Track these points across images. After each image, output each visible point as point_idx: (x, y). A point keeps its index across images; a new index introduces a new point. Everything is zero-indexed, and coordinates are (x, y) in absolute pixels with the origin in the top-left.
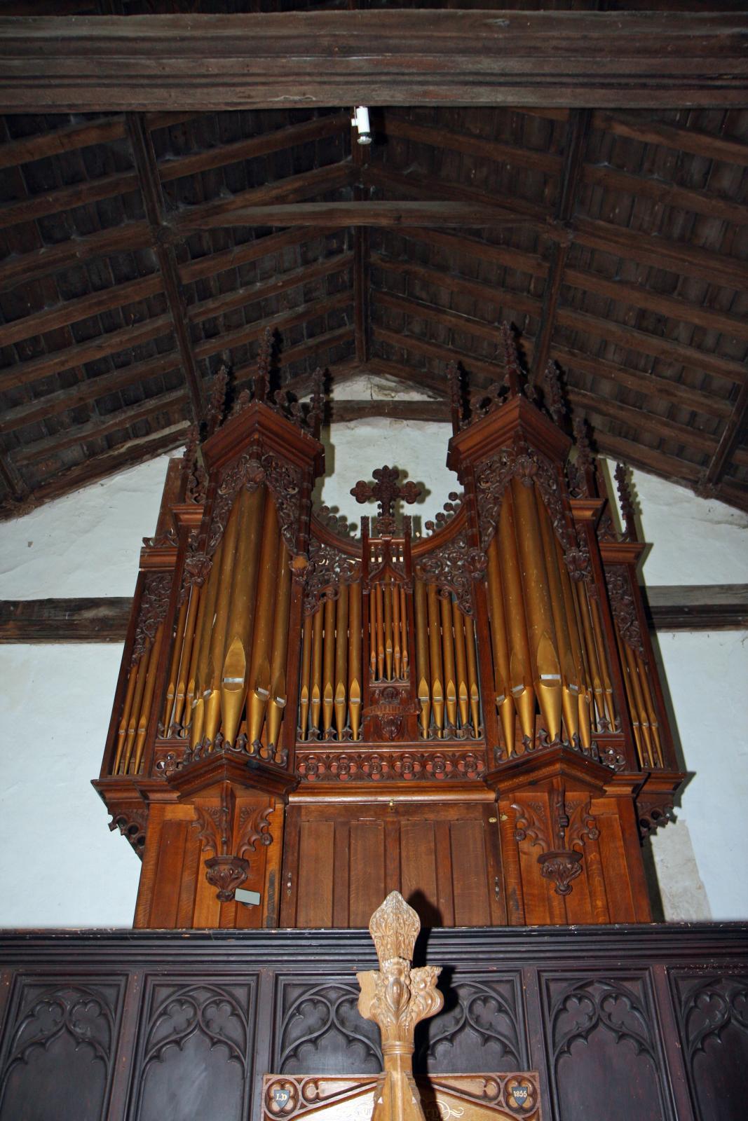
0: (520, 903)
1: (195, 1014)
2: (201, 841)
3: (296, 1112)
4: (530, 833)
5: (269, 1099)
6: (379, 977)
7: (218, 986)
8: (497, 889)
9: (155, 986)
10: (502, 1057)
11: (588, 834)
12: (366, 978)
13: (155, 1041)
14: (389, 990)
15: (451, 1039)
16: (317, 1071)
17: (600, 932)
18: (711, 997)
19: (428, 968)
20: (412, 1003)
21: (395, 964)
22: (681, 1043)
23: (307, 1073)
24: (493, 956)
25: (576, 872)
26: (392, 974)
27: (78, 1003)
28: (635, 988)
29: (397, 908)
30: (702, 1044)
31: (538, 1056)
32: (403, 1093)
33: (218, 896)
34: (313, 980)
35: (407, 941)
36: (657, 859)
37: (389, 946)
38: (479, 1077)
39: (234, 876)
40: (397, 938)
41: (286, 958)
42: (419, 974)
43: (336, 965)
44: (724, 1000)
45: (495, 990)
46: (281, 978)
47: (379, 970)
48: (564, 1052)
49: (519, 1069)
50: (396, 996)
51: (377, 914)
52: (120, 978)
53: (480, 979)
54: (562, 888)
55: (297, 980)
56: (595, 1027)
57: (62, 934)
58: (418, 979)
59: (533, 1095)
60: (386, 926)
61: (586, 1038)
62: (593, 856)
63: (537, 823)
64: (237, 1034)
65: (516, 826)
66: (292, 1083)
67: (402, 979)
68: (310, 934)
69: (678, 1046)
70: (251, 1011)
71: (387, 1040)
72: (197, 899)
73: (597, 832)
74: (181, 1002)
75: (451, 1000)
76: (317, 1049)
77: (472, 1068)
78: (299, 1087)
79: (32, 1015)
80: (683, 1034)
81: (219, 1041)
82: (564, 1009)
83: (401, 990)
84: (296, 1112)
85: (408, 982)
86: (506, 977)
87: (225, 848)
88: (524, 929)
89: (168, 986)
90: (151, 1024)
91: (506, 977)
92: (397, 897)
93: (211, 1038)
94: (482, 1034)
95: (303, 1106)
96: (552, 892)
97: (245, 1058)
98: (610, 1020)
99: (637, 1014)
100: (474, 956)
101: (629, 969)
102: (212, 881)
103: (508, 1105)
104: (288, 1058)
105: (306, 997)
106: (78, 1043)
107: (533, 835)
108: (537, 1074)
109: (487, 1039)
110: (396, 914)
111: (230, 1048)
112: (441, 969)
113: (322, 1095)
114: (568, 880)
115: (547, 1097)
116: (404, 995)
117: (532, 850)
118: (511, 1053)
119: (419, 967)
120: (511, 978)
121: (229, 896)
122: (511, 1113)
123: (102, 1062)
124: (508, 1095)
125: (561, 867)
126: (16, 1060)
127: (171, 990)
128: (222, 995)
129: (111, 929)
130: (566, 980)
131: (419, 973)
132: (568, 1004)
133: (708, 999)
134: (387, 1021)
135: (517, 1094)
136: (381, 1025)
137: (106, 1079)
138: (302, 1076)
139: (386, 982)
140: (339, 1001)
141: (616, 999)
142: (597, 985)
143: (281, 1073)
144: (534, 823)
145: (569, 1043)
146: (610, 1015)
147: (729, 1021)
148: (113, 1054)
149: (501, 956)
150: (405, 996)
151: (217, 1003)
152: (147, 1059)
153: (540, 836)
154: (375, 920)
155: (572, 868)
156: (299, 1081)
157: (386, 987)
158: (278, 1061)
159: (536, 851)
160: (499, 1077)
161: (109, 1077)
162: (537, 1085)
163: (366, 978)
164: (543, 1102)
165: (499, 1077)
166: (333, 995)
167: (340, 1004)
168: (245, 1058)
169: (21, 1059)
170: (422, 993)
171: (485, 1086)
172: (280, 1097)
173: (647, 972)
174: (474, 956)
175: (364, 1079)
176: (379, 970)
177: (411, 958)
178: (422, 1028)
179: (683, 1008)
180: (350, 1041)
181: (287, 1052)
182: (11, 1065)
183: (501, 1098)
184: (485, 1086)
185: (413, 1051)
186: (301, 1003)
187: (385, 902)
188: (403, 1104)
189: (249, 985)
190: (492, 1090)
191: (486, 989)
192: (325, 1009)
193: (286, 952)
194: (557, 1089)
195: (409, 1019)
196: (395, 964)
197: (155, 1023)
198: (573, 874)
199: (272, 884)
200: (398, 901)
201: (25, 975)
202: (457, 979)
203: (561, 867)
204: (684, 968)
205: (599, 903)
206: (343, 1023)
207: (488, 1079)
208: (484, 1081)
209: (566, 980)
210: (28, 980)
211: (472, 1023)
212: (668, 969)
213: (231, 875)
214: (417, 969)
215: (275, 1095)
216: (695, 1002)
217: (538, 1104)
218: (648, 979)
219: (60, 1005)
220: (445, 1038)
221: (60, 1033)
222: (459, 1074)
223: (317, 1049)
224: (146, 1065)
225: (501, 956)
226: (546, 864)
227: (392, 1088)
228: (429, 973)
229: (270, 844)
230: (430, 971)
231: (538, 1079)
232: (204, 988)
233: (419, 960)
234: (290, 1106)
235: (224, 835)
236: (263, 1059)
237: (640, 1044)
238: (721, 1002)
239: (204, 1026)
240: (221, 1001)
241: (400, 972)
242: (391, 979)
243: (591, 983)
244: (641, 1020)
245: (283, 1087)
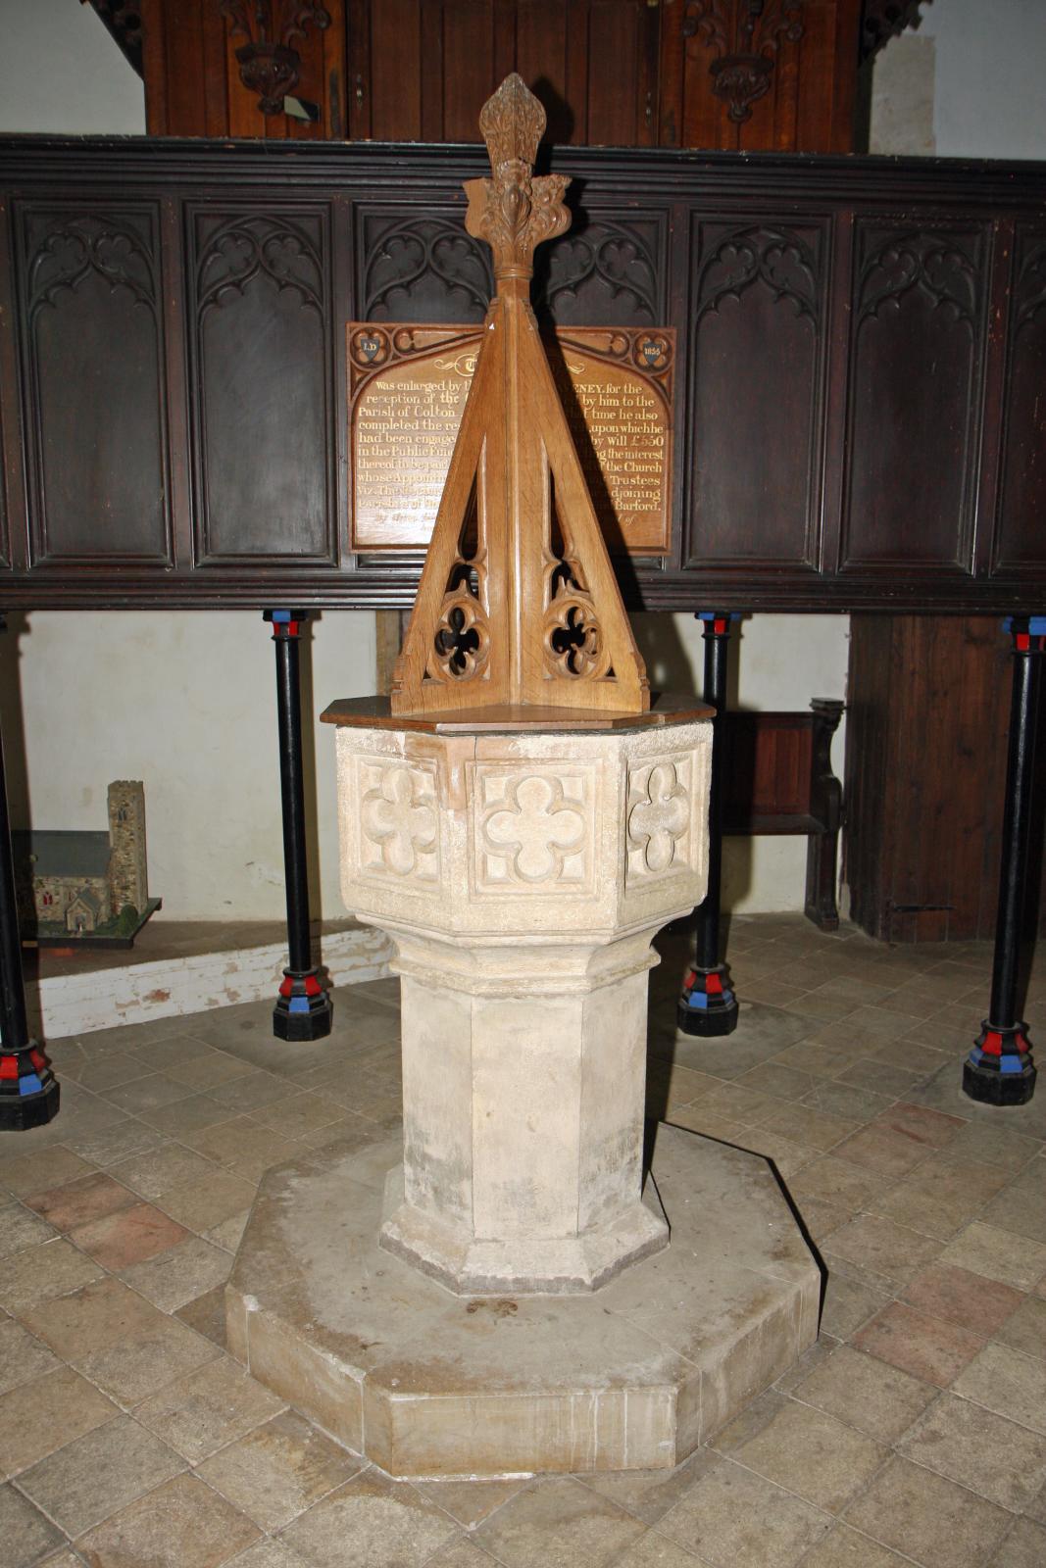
0: (678, 132)
1: (254, 250)
2: (224, 19)
3: (387, 364)
4: (705, 25)
5: (355, 349)
6: (492, 187)
7: (277, 216)
8: (648, 111)
9: (197, 216)
10: (635, 311)
11: (787, 31)
12: (475, 189)
13: (208, 283)
14: (506, 200)
15: (576, 287)
16: (412, 320)
17: (778, 162)
18: (900, 255)
19: (553, 177)
20: (532, 220)
21: (513, 167)
22: (852, 306)
23: (399, 321)
24: (636, 188)
25: (761, 88)
26: (509, 180)
27: (102, 237)
28: (810, 239)
29: (518, 101)
30: (876, 307)
31: (679, 310)
32: (518, 321)
33: (261, 107)
34: (402, 211)
35: (528, 142)
36: (877, 98)
37: (505, 147)
38: (606, 331)
39: (279, 75)
40: (516, 136)
41: (365, 182)
42: (541, 185)
43: (430, 192)
44: (916, 260)
45: (634, 232)
46: (360, 207)
47: (491, 178)
48: (711, 309)
49: (655, 325)
50: (513, 206)
51: (490, 104)
52: (149, 204)
53: (617, 218)
54: (738, 112)
55: (380, 211)
56: (751, 282)
57: (58, 140)
58: (540, 190)
59: (667, 353)
60: (501, 119)
61: (739, 295)
62: (788, 68)
63: (716, 10)
64: (311, 277)
65: (685, 13)
66: (381, 332)
67: (522, 187)
68: (396, 147)
69: (848, 307)
70: (326, 249)
71: (501, 262)
72: (231, 111)
73: (801, 29)
74: (235, 238)
75: (580, 223)
76: (410, 295)
77: (595, 322)
78: (391, 337)
79: (45, 250)
80: (856, 295)
81: (288, 284)
82: (718, 259)
83: (520, 200)
84: (387, 364)
85: (528, 193)
86: (648, 215)
87: (263, 31)
88: (679, 152)
89: (215, 216)
90: (200, 263)
91: (648, 215)
92: (516, 81)
93: (279, 281)
94: (613, 284)
95: (395, 357)
96: (724, 118)
97: (322, 303)
98: (772, 275)
99: (806, 270)
100: (611, 187)
101: (807, 215)
102: (250, 82)
103: (636, 362)
104: (374, 305)
105: (393, 232)
106: (113, 285)
107: (709, 29)
108: (675, 331)
109: (618, 290)
110: (515, 103)
111: (304, 293)
112: (570, 181)
113: (417, 346)
114: (749, 99)
115: (683, 356)
116: (523, 205)
117: (704, 54)
118: (646, 307)
119: (543, 175)
120: (656, 218)
121: (275, 106)
122: (639, 371)
123: (146, 307)
124: (637, 352)
125: (741, 80)
126: (40, 302)
127: (218, 222)
128: (286, 229)
129: (127, 136)
130: (724, 223)
131: (542, 184)
132: (723, 254)
133: (896, 256)
134: (501, 241)
135: (648, 351)
136: (493, 245)
137: (156, 324)
138: (393, 325)
139: (501, 191)
140: (436, 239)
141: (784, 250)
142: (763, 232)
143: (367, 321)
144: (712, 10)
145: (718, 299)
146: (772, 271)
147: (915, 283)
148: (158, 298)
149: (646, 188)
150: (523, 212)
151: (281, 238)
152: (202, 304)
153: (718, 30)
154: (487, 112)
155: (757, 82)
156: (390, 331)
157: (502, 197)
158: (363, 309)
159: (708, 55)
160: (629, 333)
161: (160, 323)
162: (673, 343)
163: (475, 189)
164: (677, 363)
165: (629, 333)
166: (428, 232)
167: (437, 243)
168: (322, 303)
169: (47, 300)
170: (545, 208)
171: (612, 342)
172: (368, 346)
173: (828, 220)
174: (611, 187)
175: (467, 330)
176: (491, 178)
177: (534, 162)
178: (544, 253)
179: (864, 263)
180: (451, 286)
181: (372, 298)
182: (35, 308)
183: (629, 355)
184: (612, 342)
185: (531, 275)
186: (388, 240)
187: (500, 89)
188: (518, 332)
189: (319, 216)
190: (619, 345)
191: (620, 228)
192: (419, 249)
193: (365, 173)
194: (696, 350)
195: (527, 239)
196: (513, 167)
197: (205, 261)
198: (757, 92)
199: (335, 90)
200: (518, 87)
201: (23, 198)
202: (587, 200)
203: (741, 80)
204: (876, 217)
205: (785, 139)
206: (441, 265)
207: (615, 335)
208: (610, 336)
209: (724, 223)
210: (28, 206)
211: (602, 270)
212: (855, 218)
213: (276, 73)
214: (540, 178)
215: (363, 346)
216: (881, 259)
217: (672, 363)
218: (828, 229)
219: (79, 238)
220: (567, 288)
221: (86, 274)
222: (582, 328)
223: (410, 295)
224: (202, 310)
225: (646, 188)
226: (721, 74)
227: (506, 314)
228: (554, 185)
229: (327, 27)
230: (556, 181)
231: (675, 337)
232: (262, 219)
233: (541, 168)
234: (380, 357)
235: (259, 9)
236: (344, 306)
237: (803, 304)
238: (912, 260)
239: (268, 266)
240: (285, 236)
241: (519, 178)
242: (508, 187)
243: (756, 229)
244: (810, 278)
245: (370, 336)
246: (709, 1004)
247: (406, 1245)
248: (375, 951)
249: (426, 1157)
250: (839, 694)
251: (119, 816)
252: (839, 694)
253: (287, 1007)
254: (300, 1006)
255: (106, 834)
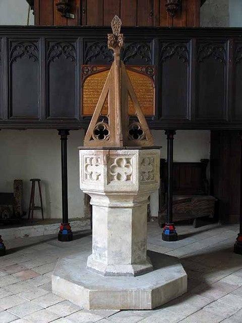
102: (59, 10)
109: (30, 57)
190: (144, 69)
246: (170, 233)
247: (92, 268)
248: (83, 226)
249: (97, 247)
250: (208, 158)
251: (17, 188)
252: (208, 158)
253: (62, 233)
254: (65, 232)
255: (12, 194)
